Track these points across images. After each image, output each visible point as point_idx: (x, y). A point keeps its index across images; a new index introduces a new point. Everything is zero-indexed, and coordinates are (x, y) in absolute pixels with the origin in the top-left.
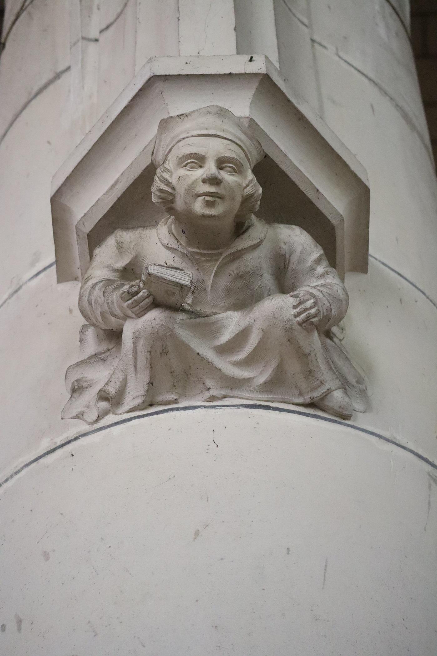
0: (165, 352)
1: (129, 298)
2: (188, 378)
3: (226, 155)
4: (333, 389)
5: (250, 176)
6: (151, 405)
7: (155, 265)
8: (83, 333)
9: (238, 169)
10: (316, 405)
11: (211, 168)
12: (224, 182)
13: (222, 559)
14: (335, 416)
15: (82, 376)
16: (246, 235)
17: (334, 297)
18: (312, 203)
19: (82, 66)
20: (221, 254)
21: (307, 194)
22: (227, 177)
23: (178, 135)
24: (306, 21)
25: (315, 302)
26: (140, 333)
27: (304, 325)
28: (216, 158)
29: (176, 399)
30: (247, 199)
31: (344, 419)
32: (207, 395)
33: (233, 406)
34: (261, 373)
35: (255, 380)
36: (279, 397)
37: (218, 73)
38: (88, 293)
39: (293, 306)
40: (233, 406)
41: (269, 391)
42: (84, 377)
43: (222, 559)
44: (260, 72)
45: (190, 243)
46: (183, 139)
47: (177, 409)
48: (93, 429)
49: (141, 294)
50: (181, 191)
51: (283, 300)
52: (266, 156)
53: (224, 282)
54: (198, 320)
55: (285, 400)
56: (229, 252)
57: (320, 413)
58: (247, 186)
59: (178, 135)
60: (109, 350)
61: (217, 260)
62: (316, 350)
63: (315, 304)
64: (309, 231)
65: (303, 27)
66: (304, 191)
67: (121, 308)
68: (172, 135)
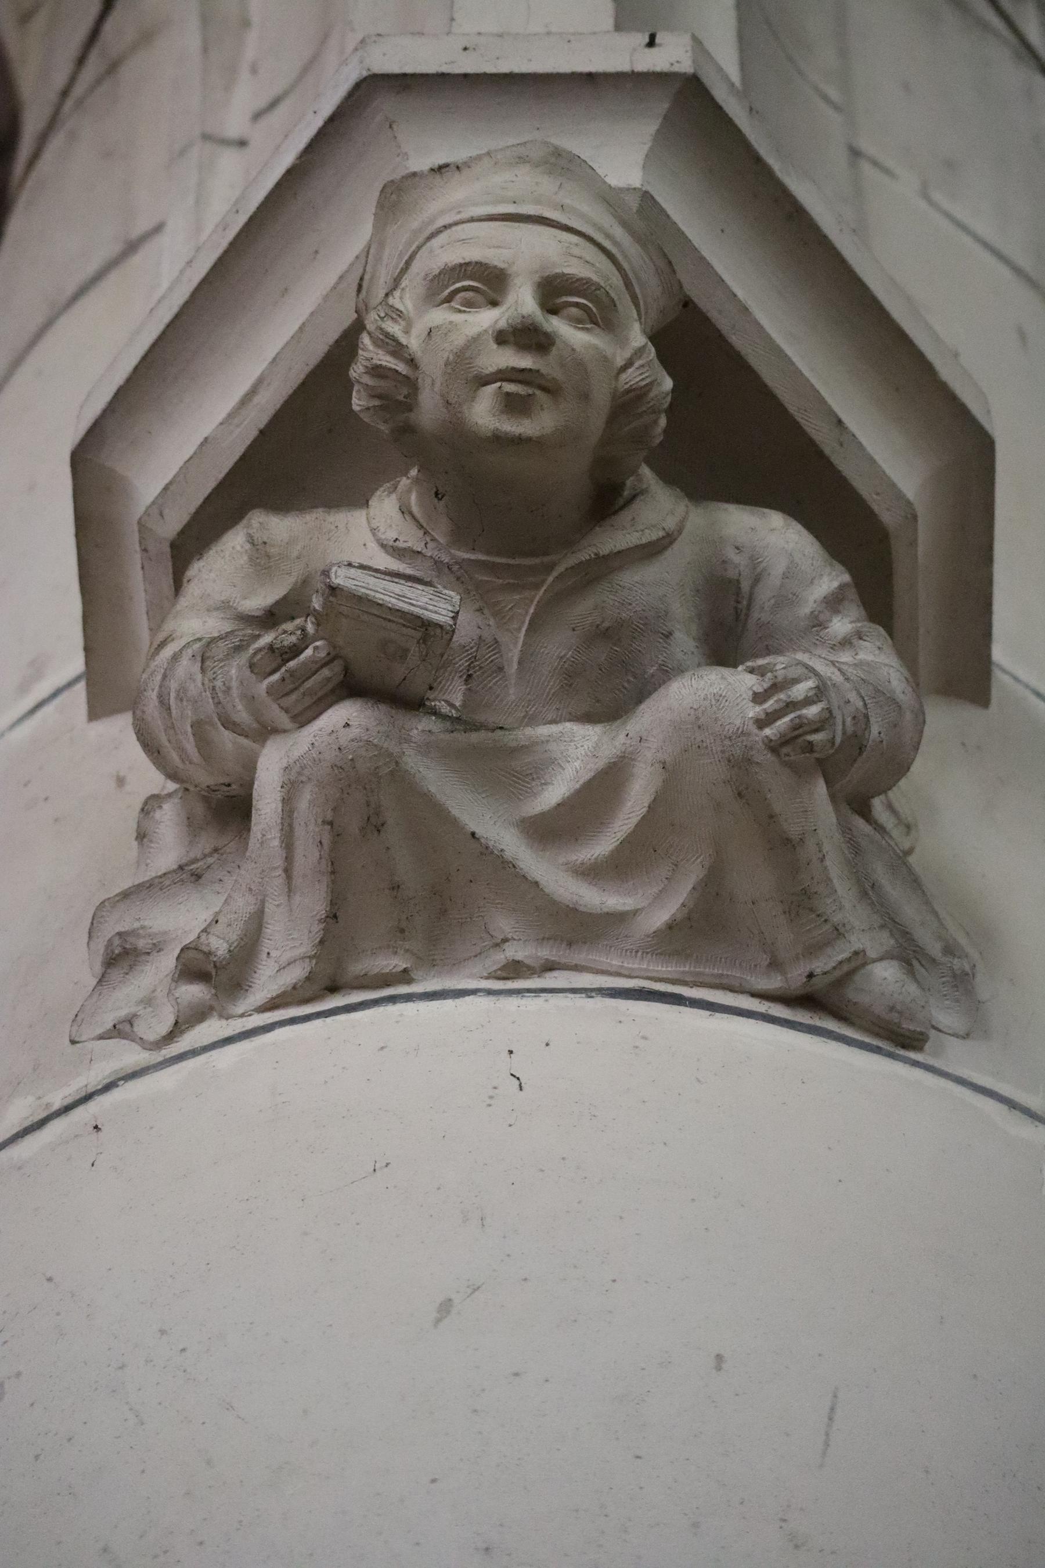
0: (374, 825)
1: (274, 665)
2: (444, 912)
3: (567, 271)
4: (872, 954)
5: (637, 337)
6: (333, 989)
7: (350, 565)
8: (148, 813)
9: (600, 315)
10: (821, 1002)
11: (523, 301)
12: (558, 341)
13: (516, 1374)
14: (877, 1035)
15: (136, 925)
16: (625, 516)
17: (877, 691)
18: (820, 454)
19: (197, 202)
20: (550, 567)
21: (808, 430)
22: (571, 334)
23: (432, 221)
24: (834, 94)
25: (817, 687)
26: (303, 768)
27: (784, 750)
28: (537, 278)
29: (405, 970)
30: (628, 404)
31: (904, 1047)
32: (500, 958)
33: (574, 991)
34: (658, 897)
35: (639, 918)
36: (709, 970)
37: (555, 71)
38: (159, 677)
39: (755, 694)
40: (574, 991)
41: (679, 954)
42: (143, 927)
43: (516, 1374)
44: (676, 68)
45: (460, 535)
46: (445, 227)
47: (409, 998)
48: (161, 1059)
49: (309, 652)
50: (433, 369)
51: (723, 678)
52: (687, 303)
53: (558, 646)
54: (475, 737)
55: (725, 981)
56: (572, 561)
57: (831, 1025)
58: (629, 364)
59: (432, 221)
60: (216, 850)
61: (537, 586)
62: (820, 832)
63: (820, 692)
64: (809, 525)
65: (830, 112)
66: (798, 417)
67: (250, 700)
68: (415, 225)
